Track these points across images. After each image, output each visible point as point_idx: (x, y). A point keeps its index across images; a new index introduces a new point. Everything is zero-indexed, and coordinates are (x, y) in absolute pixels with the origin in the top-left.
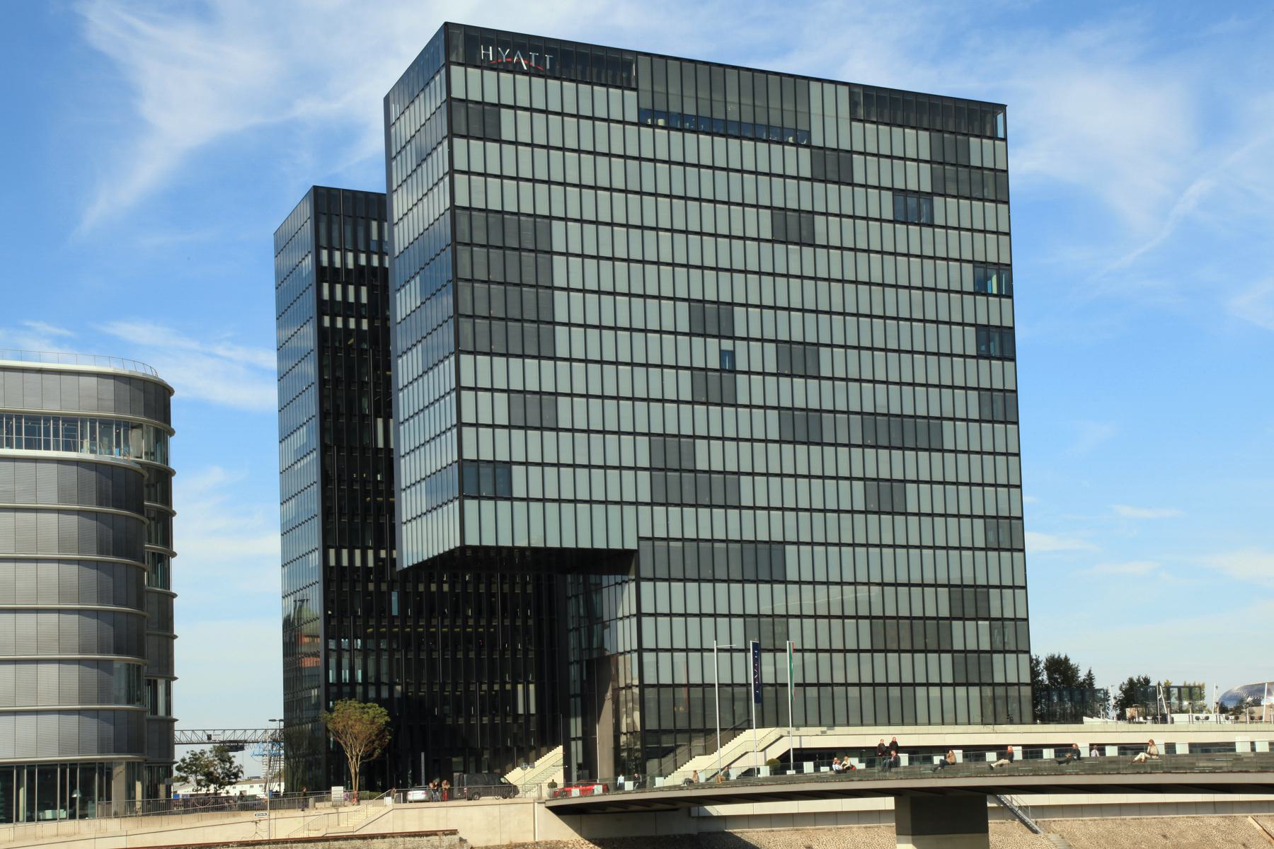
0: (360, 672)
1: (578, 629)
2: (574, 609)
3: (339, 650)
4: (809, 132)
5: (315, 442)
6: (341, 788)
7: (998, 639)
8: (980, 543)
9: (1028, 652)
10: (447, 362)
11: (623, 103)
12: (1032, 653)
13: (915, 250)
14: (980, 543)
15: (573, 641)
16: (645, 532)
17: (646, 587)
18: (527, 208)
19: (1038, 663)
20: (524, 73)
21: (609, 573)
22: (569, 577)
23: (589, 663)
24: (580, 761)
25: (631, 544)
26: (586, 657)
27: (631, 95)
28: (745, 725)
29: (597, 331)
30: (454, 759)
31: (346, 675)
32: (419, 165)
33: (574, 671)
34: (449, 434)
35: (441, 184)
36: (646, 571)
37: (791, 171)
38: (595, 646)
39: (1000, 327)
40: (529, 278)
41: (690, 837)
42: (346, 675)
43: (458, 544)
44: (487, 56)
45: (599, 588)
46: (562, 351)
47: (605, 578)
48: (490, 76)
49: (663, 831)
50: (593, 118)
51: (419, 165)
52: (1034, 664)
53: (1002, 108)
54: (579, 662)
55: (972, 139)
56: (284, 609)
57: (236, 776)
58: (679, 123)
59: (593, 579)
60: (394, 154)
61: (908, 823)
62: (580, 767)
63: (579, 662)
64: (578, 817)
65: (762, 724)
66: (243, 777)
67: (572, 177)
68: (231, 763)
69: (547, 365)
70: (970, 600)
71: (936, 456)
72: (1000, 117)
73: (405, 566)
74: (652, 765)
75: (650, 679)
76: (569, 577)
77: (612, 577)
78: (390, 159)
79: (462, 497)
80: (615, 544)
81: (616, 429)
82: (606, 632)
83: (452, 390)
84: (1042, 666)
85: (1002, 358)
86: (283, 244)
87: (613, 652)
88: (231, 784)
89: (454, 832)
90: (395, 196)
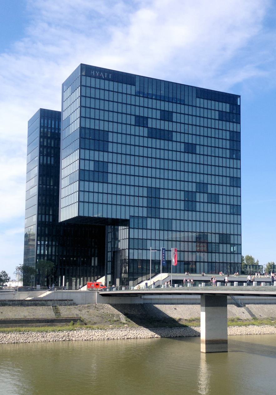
0: (46, 251)
1: (111, 242)
2: (110, 237)
3: (41, 244)
4: (184, 100)
5: (37, 183)
6: (40, 285)
7: (232, 211)
8: (228, 212)
9: (241, 254)
10: (77, 151)
11: (132, 90)
12: (242, 254)
13: (213, 136)
14: (228, 212)
15: (109, 245)
16: (132, 214)
17: (131, 230)
18: (102, 128)
19: (243, 257)
20: (103, 79)
21: (121, 226)
22: (109, 226)
23: (114, 252)
24: (110, 280)
25: (128, 218)
26: (113, 250)
27: (133, 87)
28: (158, 272)
29: (120, 175)
30: (73, 278)
31: (42, 252)
32: (71, 94)
33: (109, 254)
34: (76, 193)
35: (77, 110)
36: (132, 226)
37: (178, 115)
38: (116, 247)
39: (237, 132)
40: (101, 139)
41: (141, 304)
42: (42, 252)
43: (77, 215)
44: (92, 74)
45: (118, 230)
46: (110, 181)
47: (119, 227)
48: (93, 79)
49: (133, 302)
50: (122, 123)
51: (71, 94)
52: (242, 257)
53: (240, 96)
54: (111, 252)
55: (229, 112)
56: (25, 231)
57: (8, 279)
58: (147, 96)
59: (116, 227)
60: (64, 110)
61: (204, 303)
62: (110, 282)
63: (111, 252)
64: (108, 297)
65: (163, 272)
66: (11, 280)
67: (115, 120)
68: (7, 276)
69: (106, 154)
70: (225, 239)
71: (217, 205)
72: (239, 99)
73: (61, 221)
74: (131, 283)
75: (131, 236)
76: (109, 226)
77: (122, 227)
78: (63, 102)
79: (80, 180)
80: (123, 218)
81: (125, 174)
82: (119, 243)
83: (78, 118)
84: (244, 258)
85: (237, 187)
86: (31, 122)
87: (121, 249)
88: (7, 282)
89: (72, 300)
90: (64, 112)
